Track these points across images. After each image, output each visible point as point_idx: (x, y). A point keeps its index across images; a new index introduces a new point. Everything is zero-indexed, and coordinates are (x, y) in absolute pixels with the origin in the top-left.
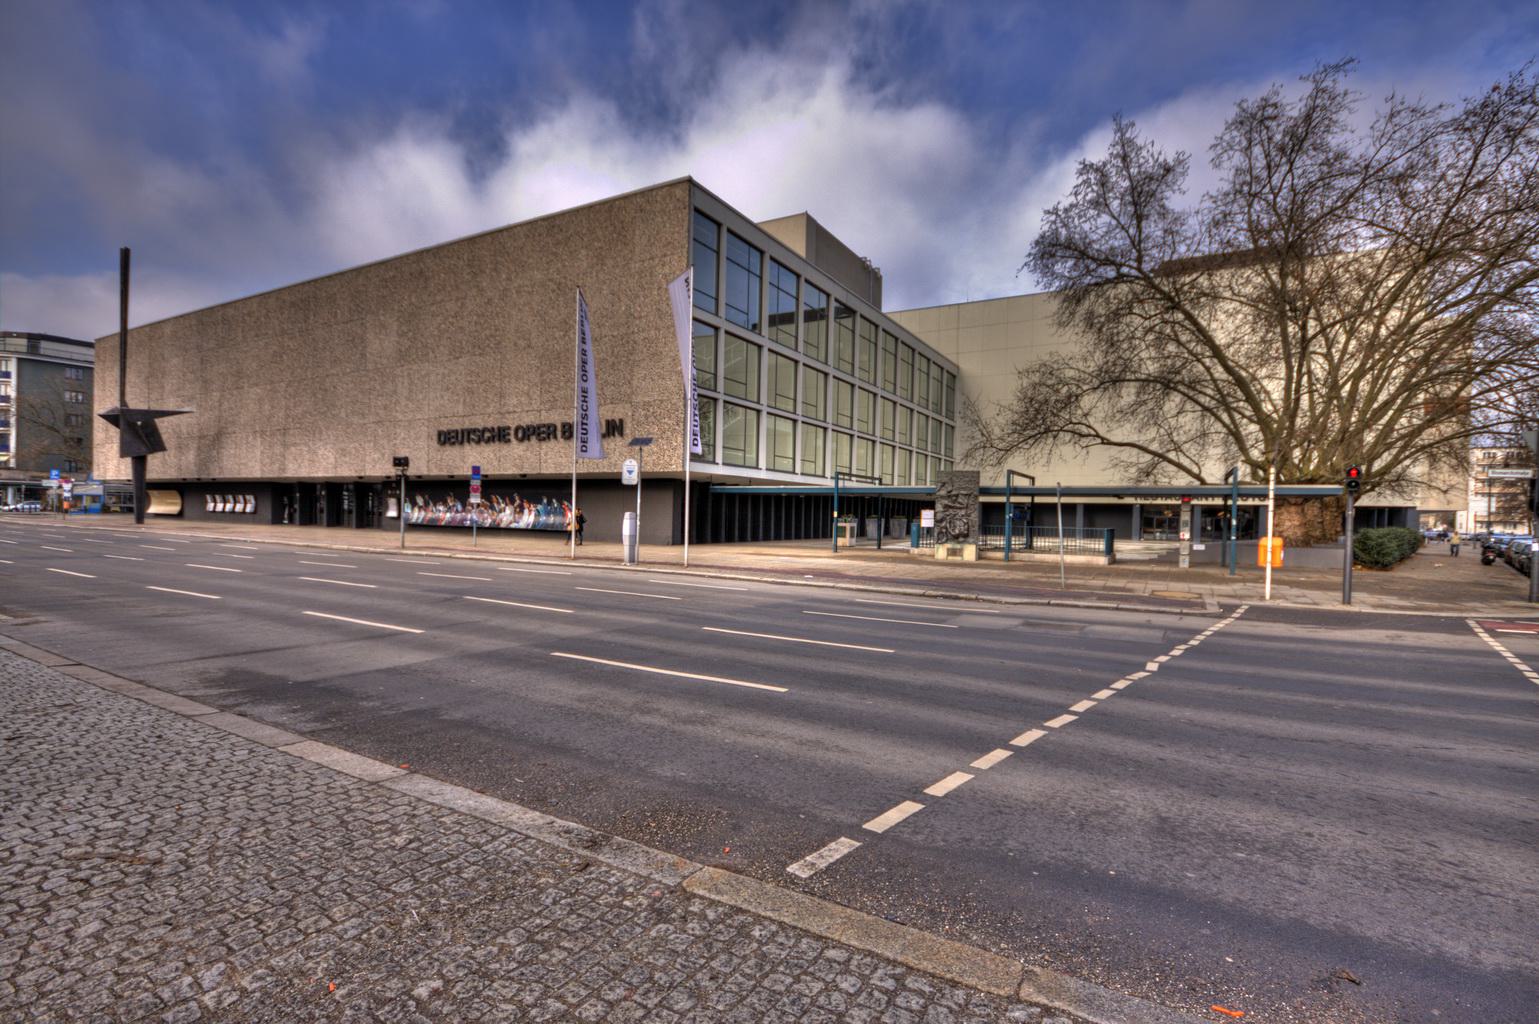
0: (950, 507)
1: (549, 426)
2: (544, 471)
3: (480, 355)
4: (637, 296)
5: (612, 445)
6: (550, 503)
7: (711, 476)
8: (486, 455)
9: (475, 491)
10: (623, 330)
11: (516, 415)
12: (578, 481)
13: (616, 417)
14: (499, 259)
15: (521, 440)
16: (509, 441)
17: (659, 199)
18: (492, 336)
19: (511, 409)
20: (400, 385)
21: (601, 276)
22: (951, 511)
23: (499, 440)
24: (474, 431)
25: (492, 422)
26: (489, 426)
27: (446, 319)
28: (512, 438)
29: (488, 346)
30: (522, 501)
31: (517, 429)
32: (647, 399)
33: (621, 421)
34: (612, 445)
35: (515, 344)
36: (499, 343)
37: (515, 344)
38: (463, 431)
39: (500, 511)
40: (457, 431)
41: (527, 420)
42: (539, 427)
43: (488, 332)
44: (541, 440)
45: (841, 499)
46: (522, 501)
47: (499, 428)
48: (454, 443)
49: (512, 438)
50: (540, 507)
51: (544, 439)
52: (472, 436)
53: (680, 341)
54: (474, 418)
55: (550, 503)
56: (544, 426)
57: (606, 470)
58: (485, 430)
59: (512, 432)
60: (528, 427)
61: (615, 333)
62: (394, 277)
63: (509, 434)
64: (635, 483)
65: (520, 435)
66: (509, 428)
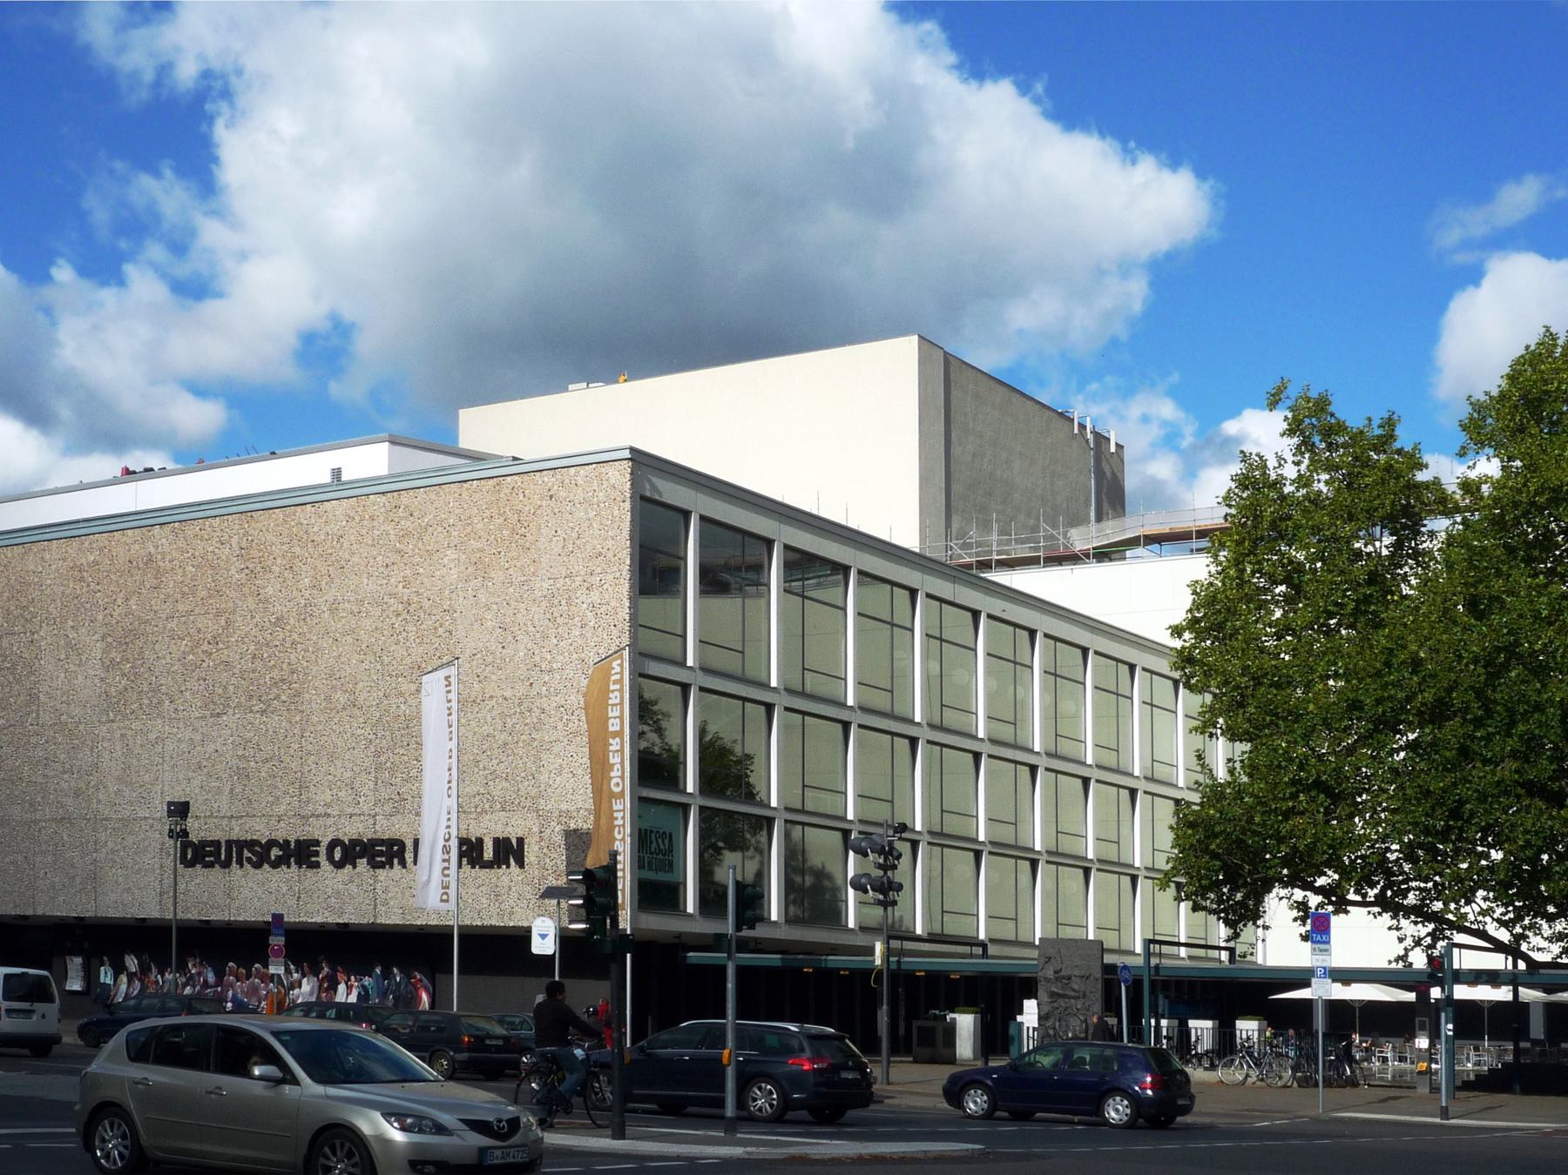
0: (1059, 995)
1: (391, 843)
2: (381, 920)
3: (263, 712)
4: (545, 637)
5: (505, 879)
6: (387, 974)
7: (679, 935)
8: (273, 886)
9: (277, 954)
10: (521, 689)
11: (330, 821)
12: (460, 936)
13: (513, 833)
14: (297, 550)
15: (339, 865)
16: (317, 865)
17: (580, 481)
18: (283, 681)
19: (321, 810)
20: (106, 755)
21: (483, 597)
22: (1062, 1002)
23: (299, 864)
24: (251, 844)
25: (289, 832)
26: (280, 836)
27: (198, 645)
28: (322, 859)
29: (277, 697)
30: (334, 971)
31: (334, 843)
32: (564, 807)
33: (521, 841)
34: (505, 879)
35: (328, 699)
36: (298, 694)
37: (328, 699)
38: (229, 843)
39: (292, 987)
40: (217, 844)
41: (352, 830)
42: (374, 842)
43: (275, 673)
44: (375, 866)
45: (179, 929)
46: (334, 971)
47: (298, 842)
48: (210, 865)
49: (322, 859)
50: (367, 981)
51: (382, 866)
52: (246, 854)
53: (744, 803)
54: (250, 823)
55: (387, 974)
56: (382, 842)
57: (494, 922)
58: (272, 843)
59: (323, 850)
60: (355, 843)
61: (508, 694)
62: (96, 563)
63: (317, 854)
64: (550, 952)
65: (337, 855)
66: (317, 843)
